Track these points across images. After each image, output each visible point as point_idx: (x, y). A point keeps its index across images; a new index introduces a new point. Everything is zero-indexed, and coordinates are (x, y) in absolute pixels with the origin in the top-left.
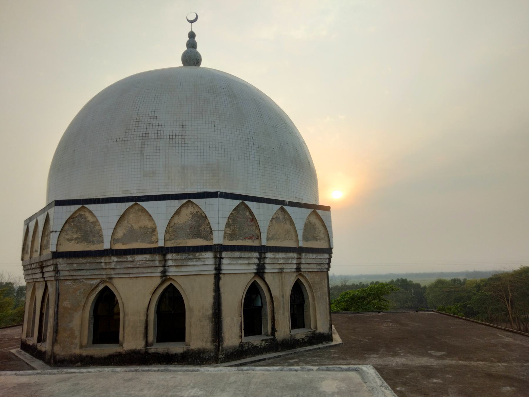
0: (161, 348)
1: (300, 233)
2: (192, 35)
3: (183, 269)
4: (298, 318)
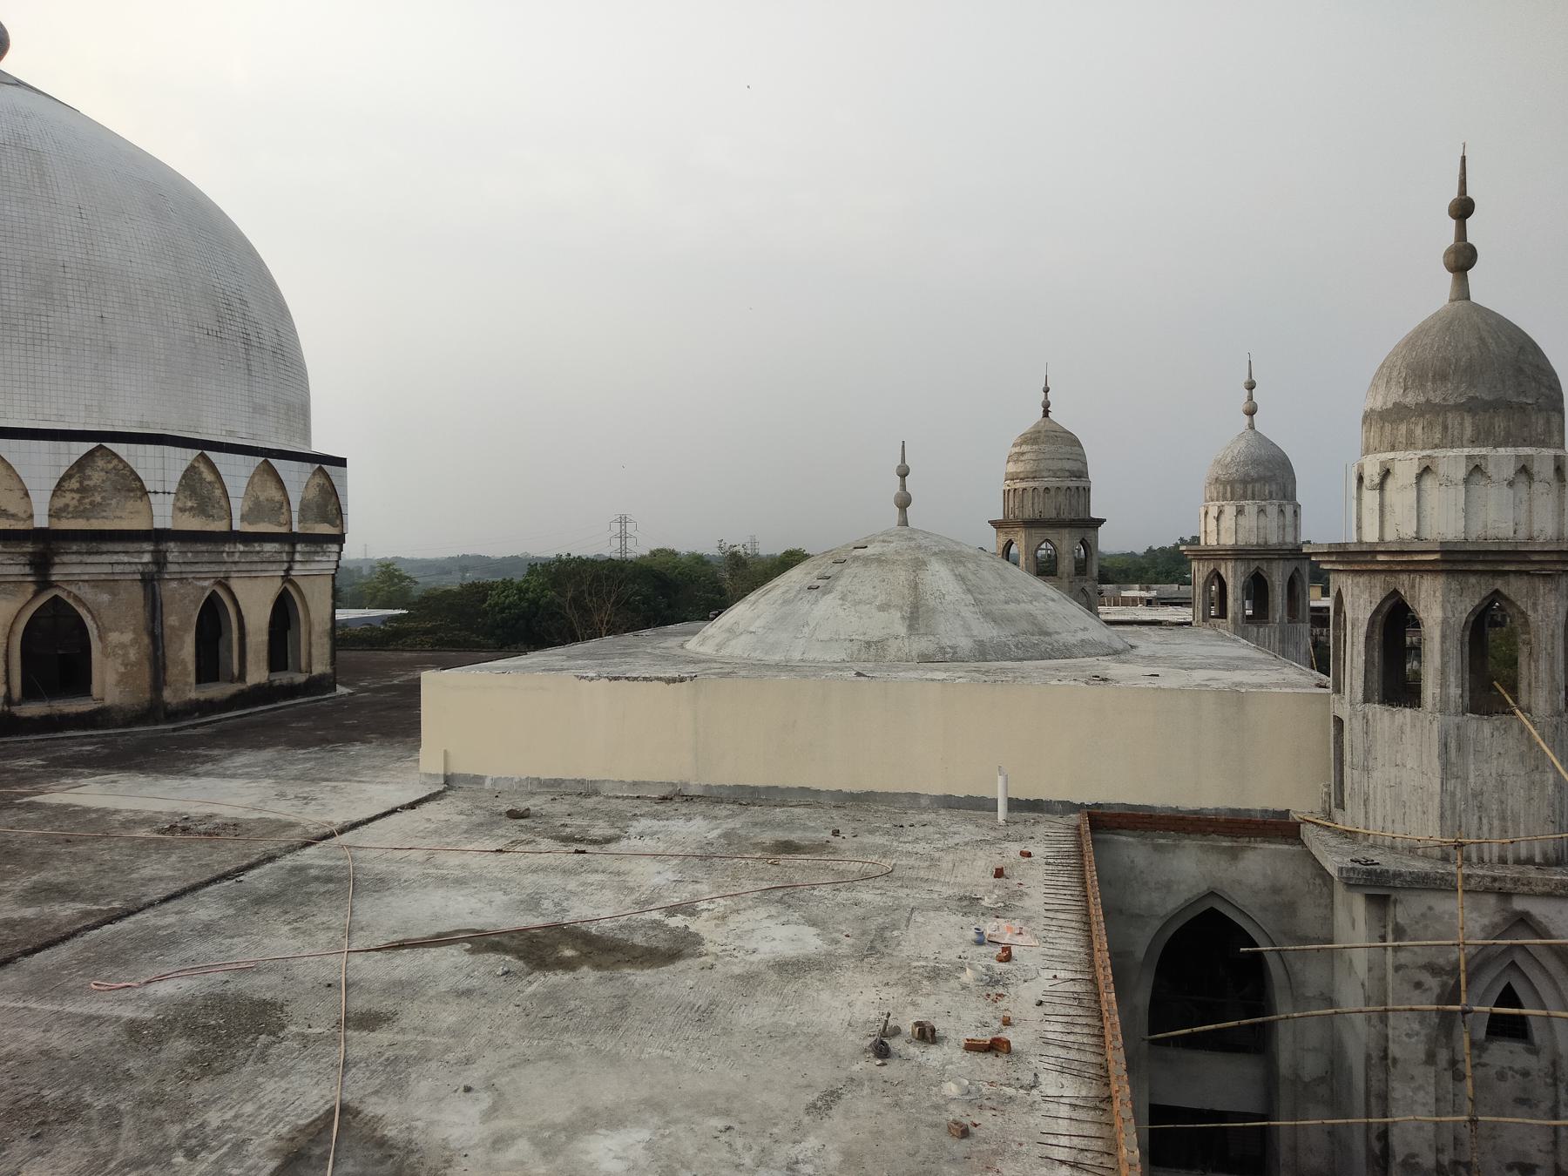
1: (295, 506)
3: (308, 567)
4: (279, 654)
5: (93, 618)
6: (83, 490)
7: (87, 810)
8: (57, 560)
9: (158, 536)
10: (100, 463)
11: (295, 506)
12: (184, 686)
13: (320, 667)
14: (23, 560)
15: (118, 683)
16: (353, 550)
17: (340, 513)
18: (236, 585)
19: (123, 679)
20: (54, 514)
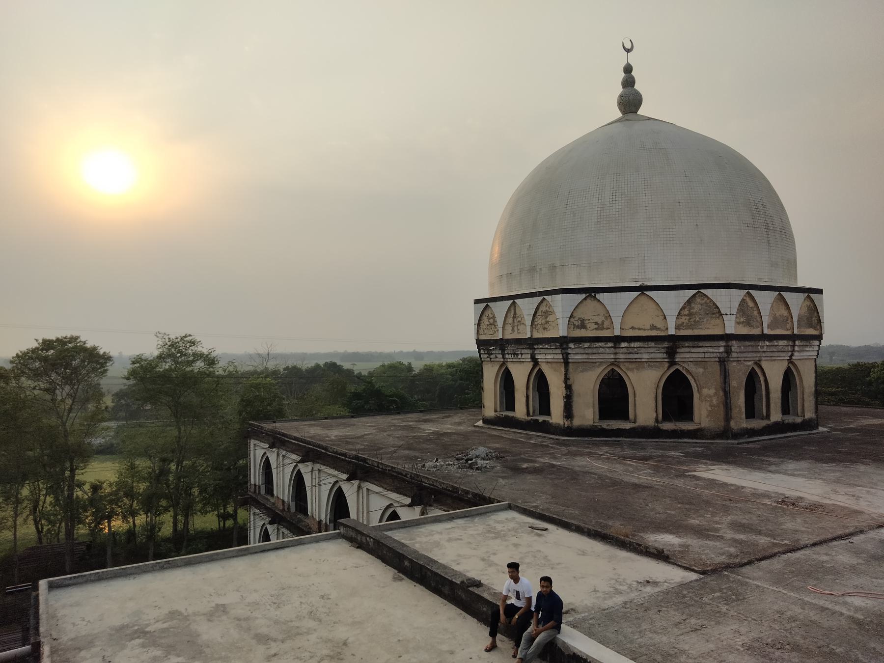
0: (668, 426)
1: (795, 319)
2: (628, 69)
5: (695, 381)
6: (690, 315)
7: (726, 484)
8: (678, 350)
9: (727, 338)
10: (698, 300)
11: (795, 319)
12: (740, 422)
13: (809, 414)
14: (663, 350)
15: (707, 417)
16: (824, 343)
17: (819, 321)
18: (764, 365)
19: (710, 414)
20: (677, 328)
